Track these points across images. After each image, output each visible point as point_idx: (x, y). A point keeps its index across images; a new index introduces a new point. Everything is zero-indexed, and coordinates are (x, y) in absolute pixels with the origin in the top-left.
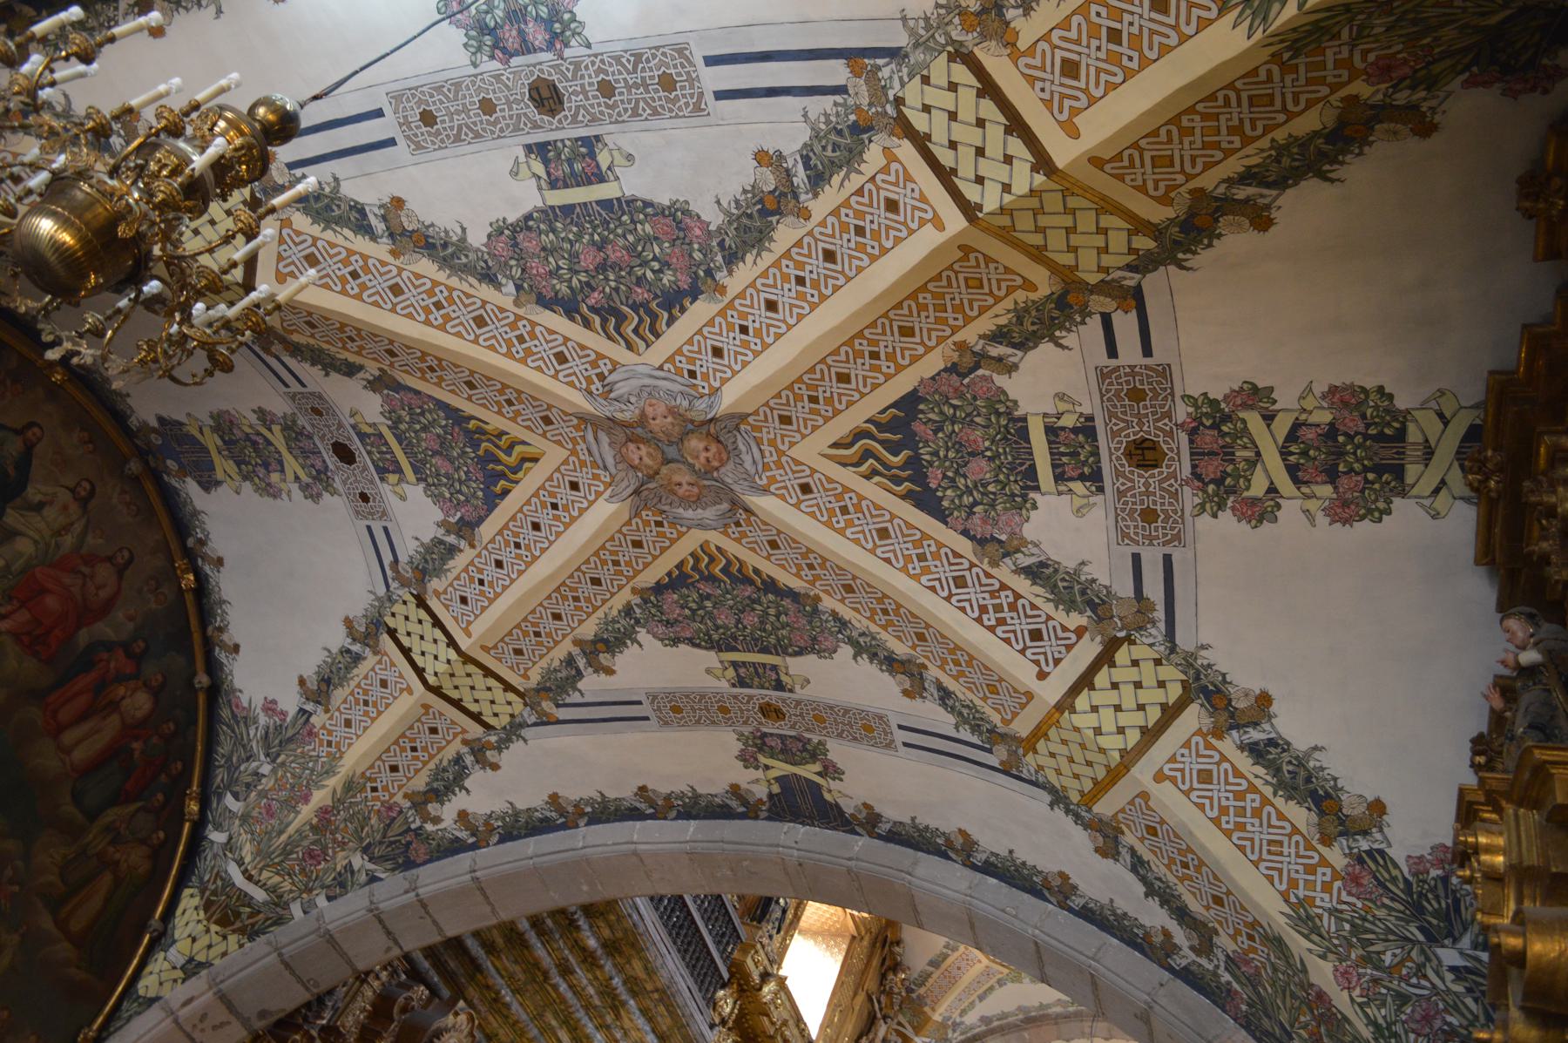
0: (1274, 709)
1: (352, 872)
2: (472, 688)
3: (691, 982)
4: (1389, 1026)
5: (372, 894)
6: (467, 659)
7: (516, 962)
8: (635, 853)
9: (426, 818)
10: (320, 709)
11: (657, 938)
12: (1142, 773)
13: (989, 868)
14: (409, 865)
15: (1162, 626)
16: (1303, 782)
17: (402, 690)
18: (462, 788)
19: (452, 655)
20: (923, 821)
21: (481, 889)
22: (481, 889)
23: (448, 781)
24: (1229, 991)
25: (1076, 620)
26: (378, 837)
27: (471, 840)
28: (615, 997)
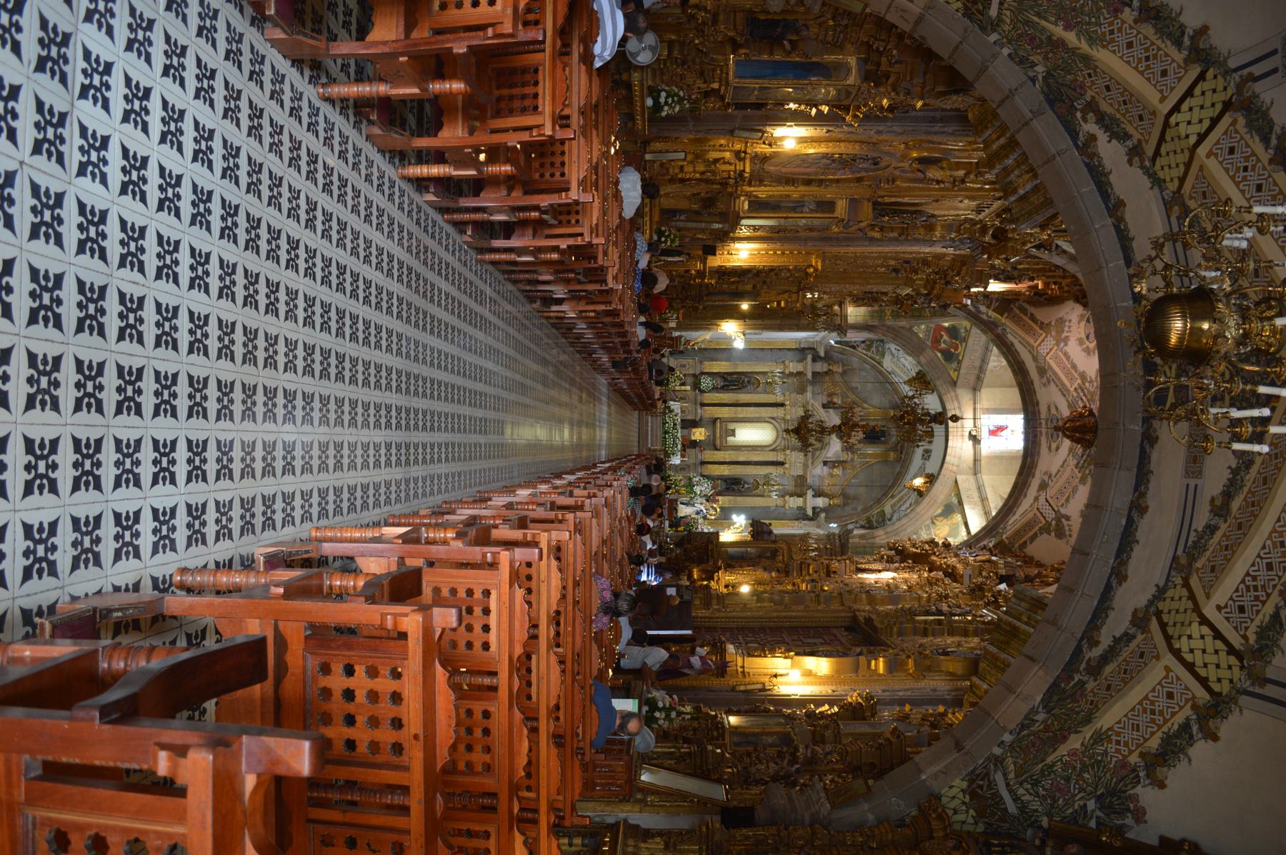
0: (1210, 742)
1: (1032, 67)
10: (1136, 13)
12: (1169, 660)
14: (1051, 103)
15: (1251, 689)
16: (1173, 749)
20: (1153, 479)
25: (1252, 638)
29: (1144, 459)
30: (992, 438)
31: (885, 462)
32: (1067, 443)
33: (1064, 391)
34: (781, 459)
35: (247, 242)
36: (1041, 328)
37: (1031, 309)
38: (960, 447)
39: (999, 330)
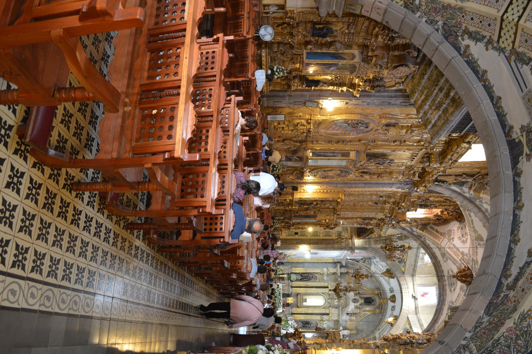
1: (436, 23)
2: (508, 31)
3: (455, 125)
4: (500, 343)
5: (433, 32)
6: (517, 25)
7: (436, 75)
8: (479, 104)
9: (462, 36)
11: (463, 111)
13: (515, 216)
14: (446, 38)
17: (497, 8)
18: (476, 42)
19: (516, 20)
20: (523, 191)
21: (449, 63)
22: (449, 63)
23: (476, 37)
24: (498, 296)
26: (450, 25)
27: (462, 52)
28: (440, 107)
29: (516, 184)
30: (422, 297)
31: (374, 314)
32: (459, 284)
33: (454, 262)
34: (327, 312)
35: (105, 238)
36: (441, 235)
37: (436, 228)
38: (408, 304)
39: (422, 239)
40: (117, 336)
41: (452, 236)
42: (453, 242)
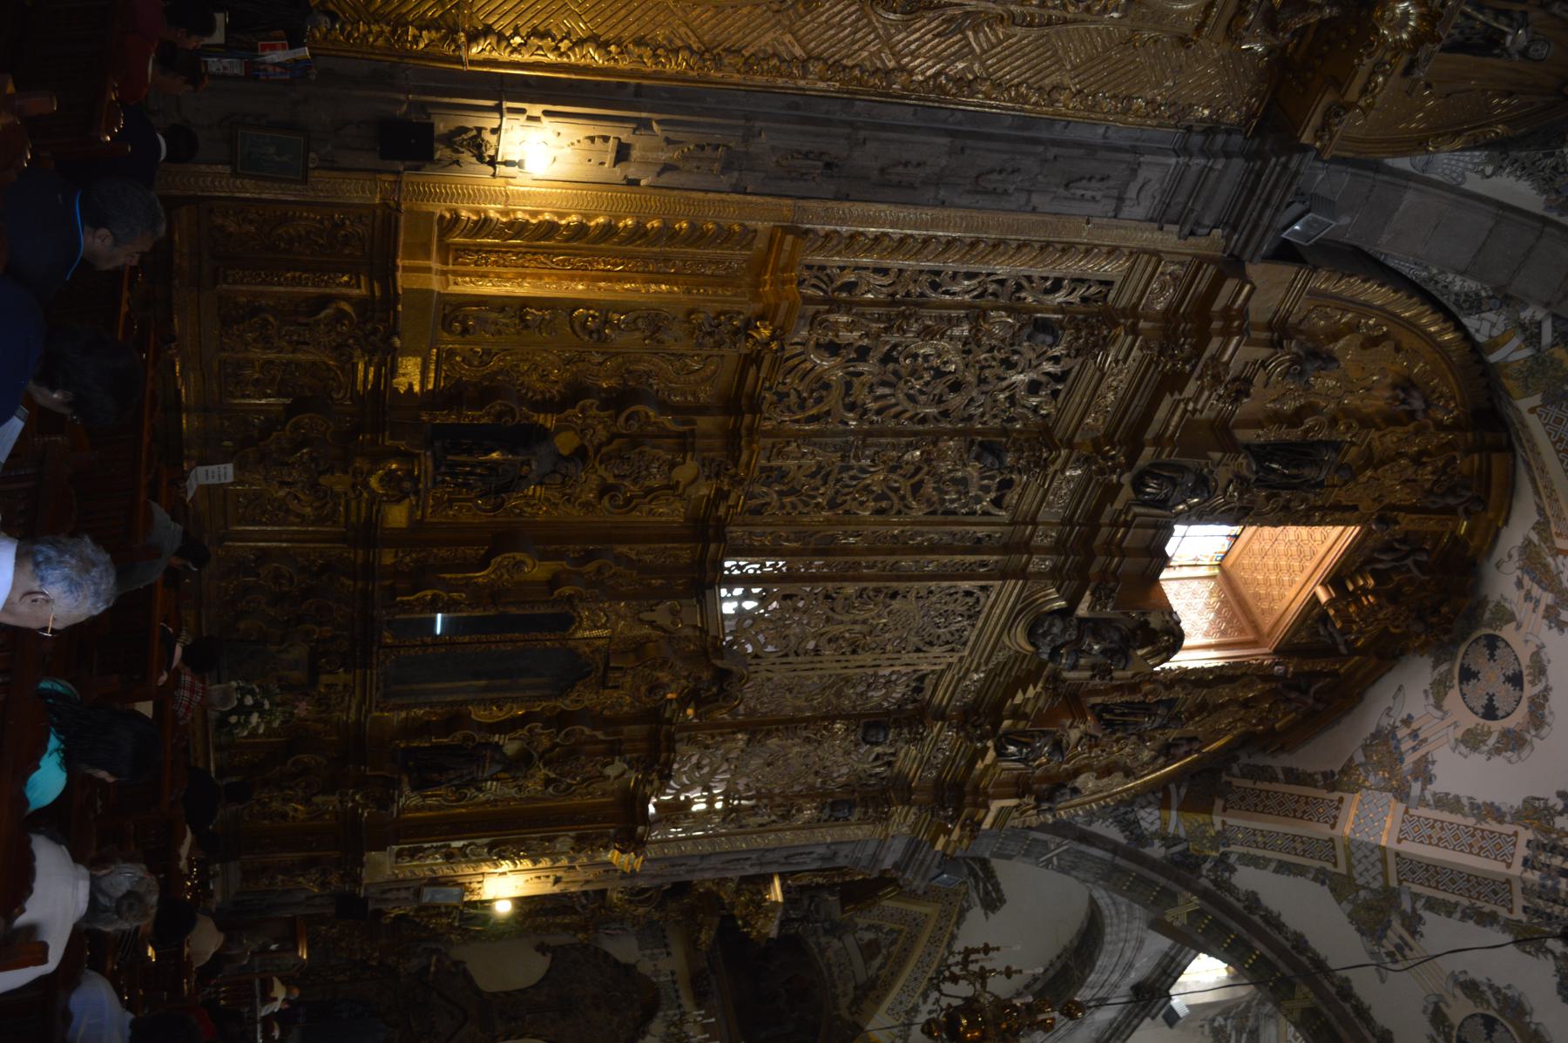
36: (1332, 788)
37: (1280, 762)
40: (477, 146)
41: (1410, 759)
42: (1437, 787)
